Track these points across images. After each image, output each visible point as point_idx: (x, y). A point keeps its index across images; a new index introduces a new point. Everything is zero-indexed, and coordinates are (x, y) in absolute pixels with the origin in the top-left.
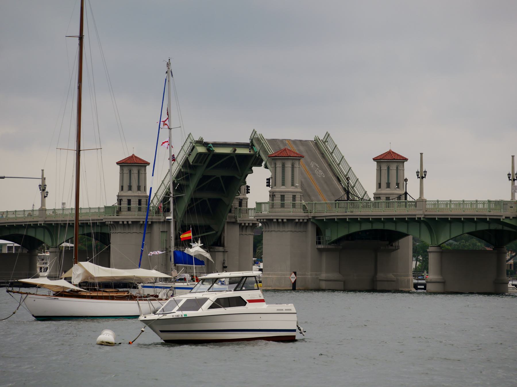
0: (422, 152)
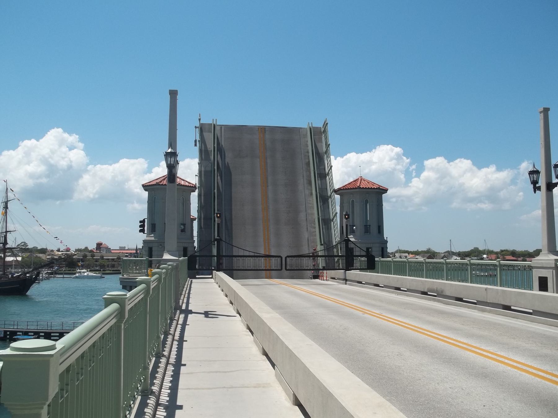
0: (195, 147)
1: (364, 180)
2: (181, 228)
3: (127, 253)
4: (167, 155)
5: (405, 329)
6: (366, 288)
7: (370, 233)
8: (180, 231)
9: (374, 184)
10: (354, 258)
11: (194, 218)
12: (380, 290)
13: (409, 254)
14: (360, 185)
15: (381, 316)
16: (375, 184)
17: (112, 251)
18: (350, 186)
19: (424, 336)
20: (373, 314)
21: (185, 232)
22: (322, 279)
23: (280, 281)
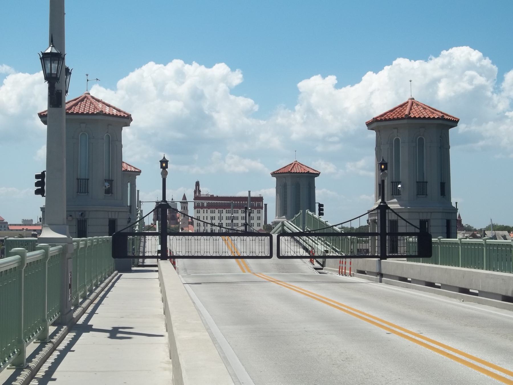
1: (417, 105)
2: (106, 187)
3: (35, 230)
4: (45, 57)
5: (452, 360)
6: (413, 289)
7: (426, 195)
8: (104, 192)
9: (435, 112)
10: (399, 237)
11: (137, 170)
12: (435, 293)
13: (509, 232)
14: (410, 113)
15: (417, 338)
16: (435, 110)
17: (11, 228)
18: (393, 115)
19: (482, 374)
20: (407, 334)
21: (112, 193)
22: (343, 273)
23: (272, 277)
